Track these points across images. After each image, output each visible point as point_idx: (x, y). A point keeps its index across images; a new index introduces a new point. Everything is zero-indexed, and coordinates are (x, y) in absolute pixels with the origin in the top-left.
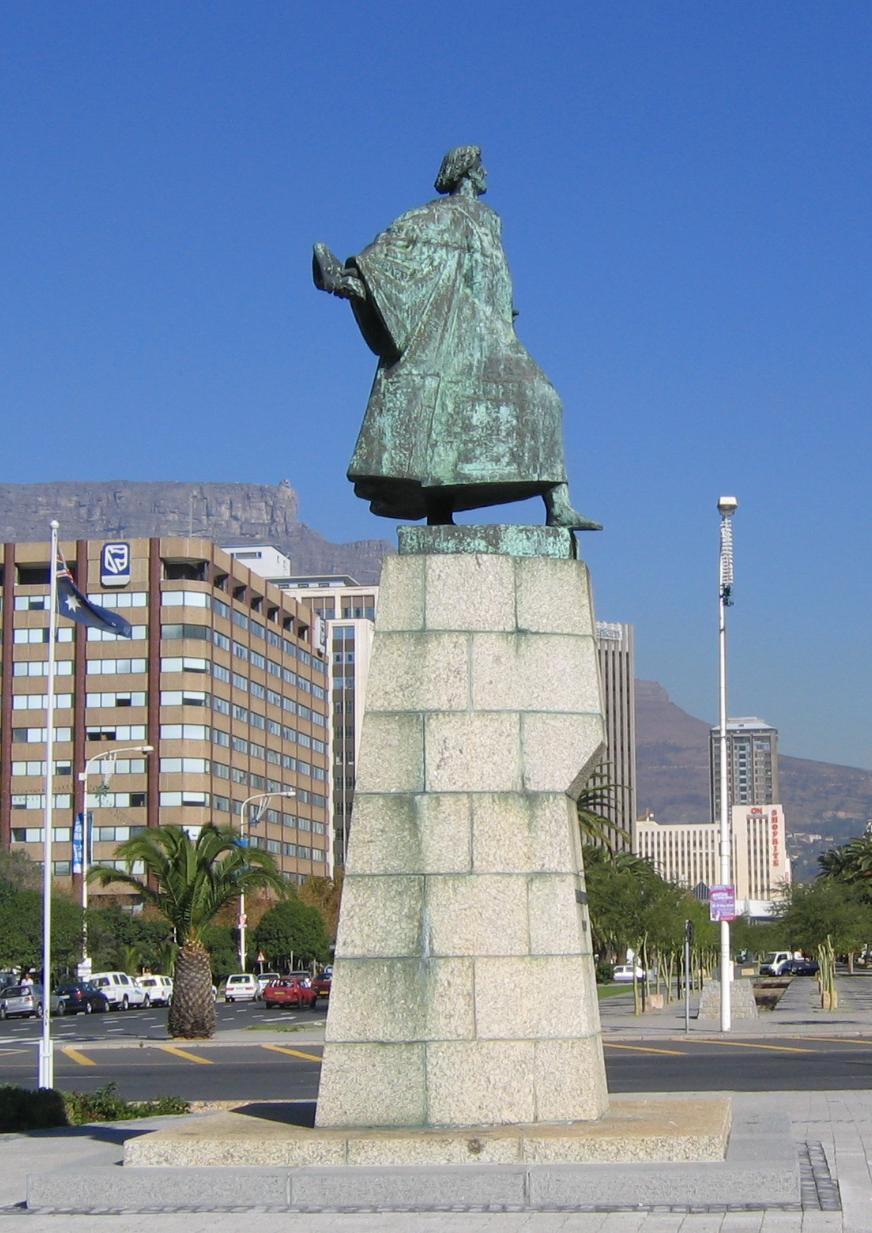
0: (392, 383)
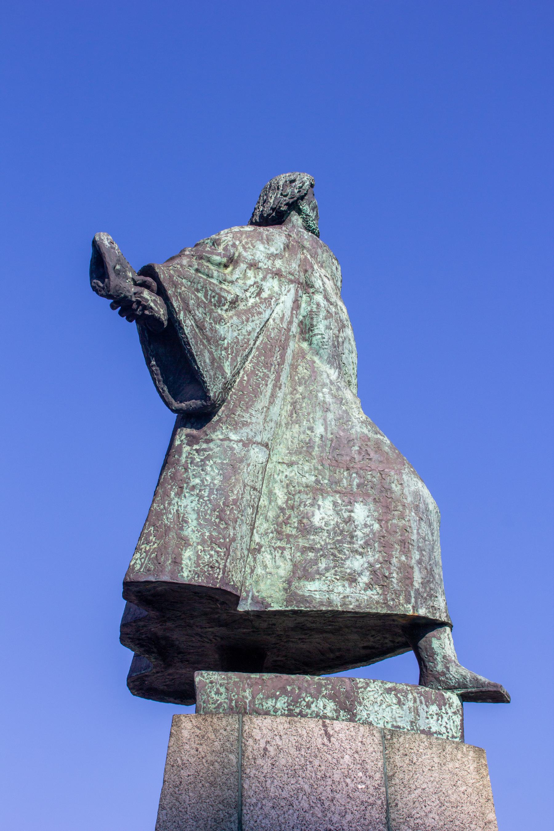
0: (197, 451)
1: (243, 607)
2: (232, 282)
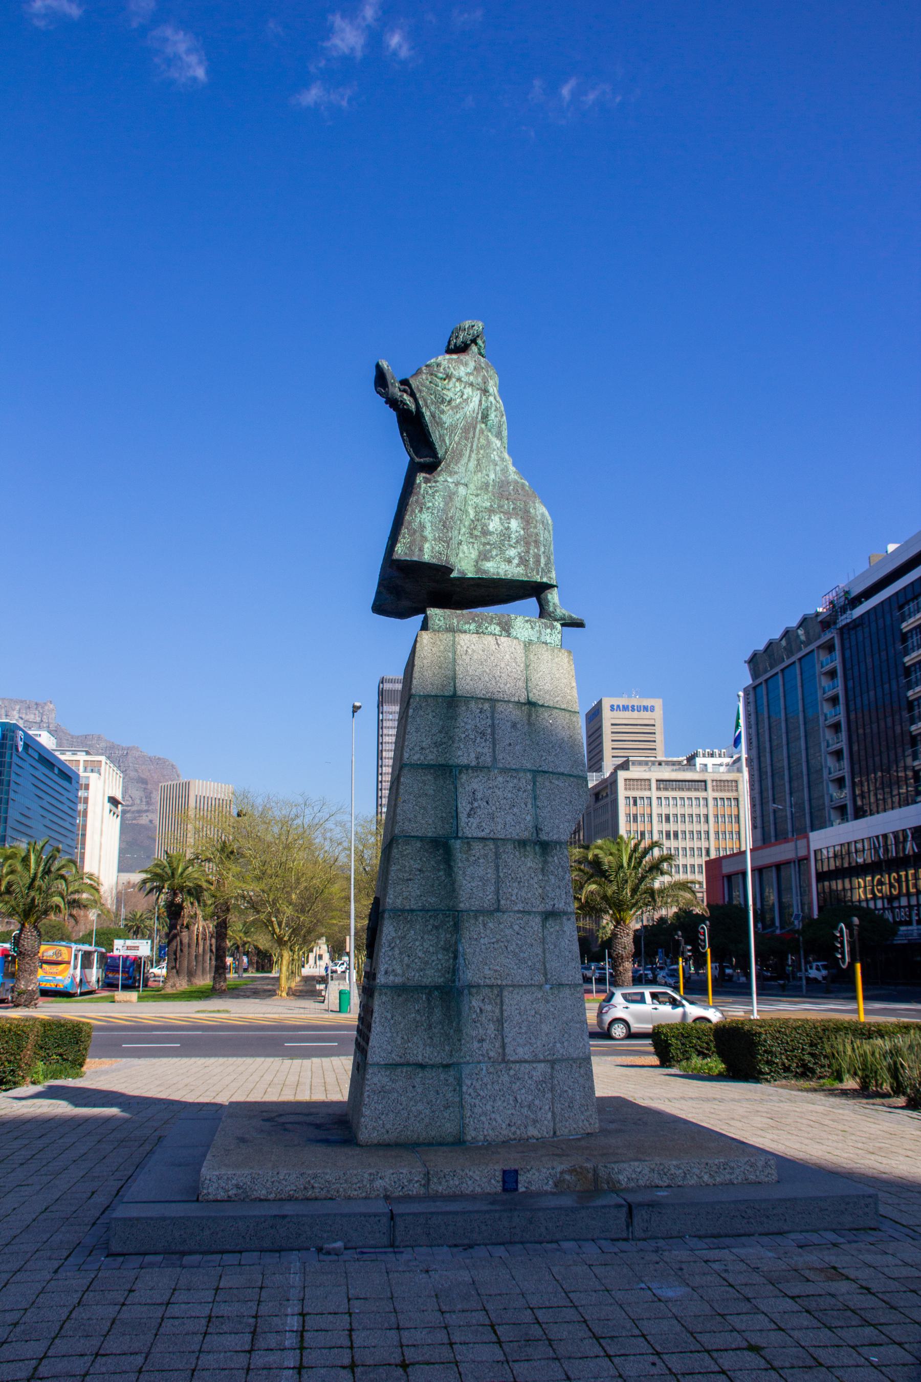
0: (430, 487)
1: (454, 575)
2: (449, 390)
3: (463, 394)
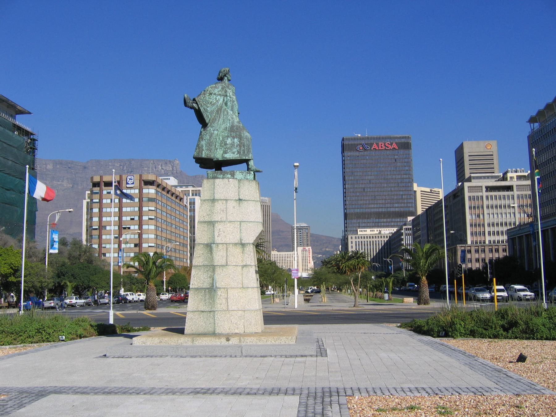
3: (216, 99)
